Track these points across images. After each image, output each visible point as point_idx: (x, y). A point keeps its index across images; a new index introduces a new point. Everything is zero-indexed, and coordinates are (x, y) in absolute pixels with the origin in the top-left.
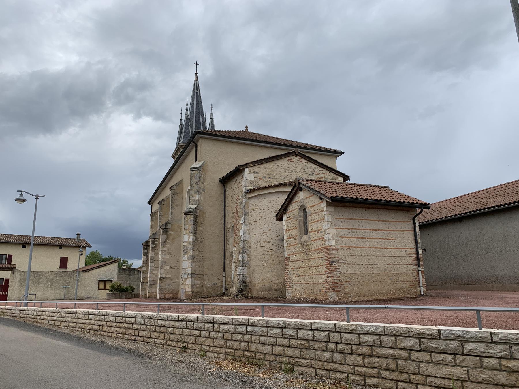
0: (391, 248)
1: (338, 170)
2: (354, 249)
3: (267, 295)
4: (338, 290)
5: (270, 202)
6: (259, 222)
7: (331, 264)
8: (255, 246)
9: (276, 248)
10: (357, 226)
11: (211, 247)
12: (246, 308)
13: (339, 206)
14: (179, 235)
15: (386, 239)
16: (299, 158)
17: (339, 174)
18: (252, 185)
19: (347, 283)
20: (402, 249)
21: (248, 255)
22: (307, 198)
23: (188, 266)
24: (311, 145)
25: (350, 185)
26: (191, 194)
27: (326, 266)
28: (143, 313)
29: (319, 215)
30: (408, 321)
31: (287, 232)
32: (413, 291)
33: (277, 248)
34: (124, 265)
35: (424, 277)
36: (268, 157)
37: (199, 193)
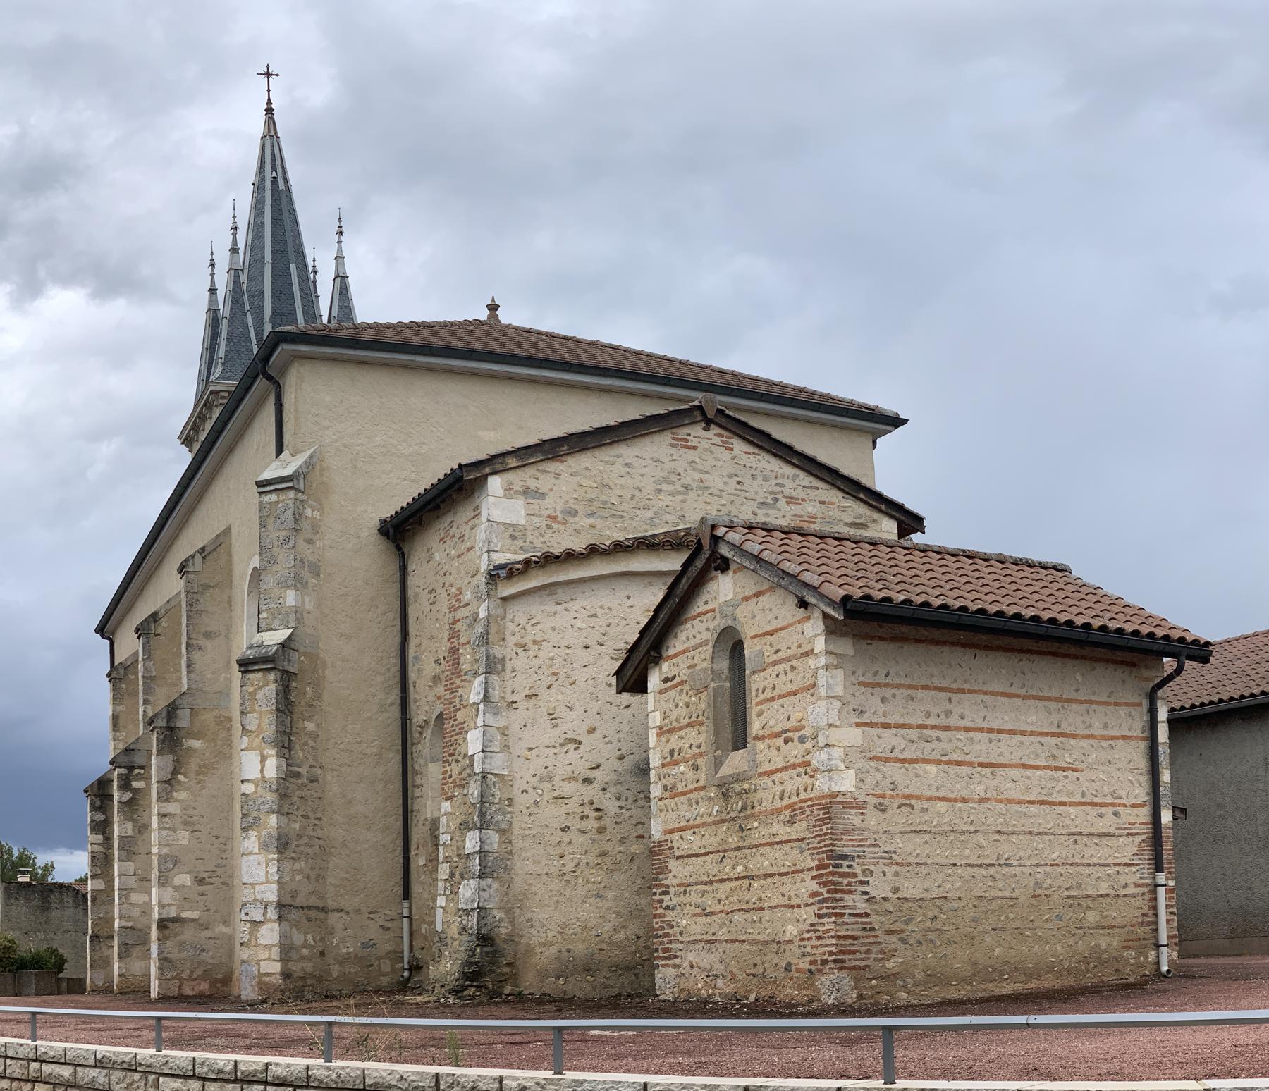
0: (1064, 804)
1: (879, 487)
2: (925, 805)
3: (578, 987)
4: (858, 963)
5: (595, 616)
6: (549, 699)
7: (837, 866)
8: (532, 796)
9: (618, 803)
10: (943, 716)
11: (349, 802)
12: (492, 1038)
13: (873, 638)
14: (224, 754)
15: (1047, 768)
16: (718, 435)
17: (883, 507)
18: (519, 543)
19: (894, 938)
20: (1102, 805)
21: (502, 832)
22: (746, 599)
23: (263, 874)
24: (772, 383)
25: (923, 551)
26: (263, 587)
27: (815, 873)
28: (102, 1050)
29: (793, 668)
30: (1106, 1067)
31: (664, 738)
32: (1132, 961)
33: (622, 803)
34: (24, 873)
35: (1174, 910)
36: (587, 428)
37: (297, 582)
